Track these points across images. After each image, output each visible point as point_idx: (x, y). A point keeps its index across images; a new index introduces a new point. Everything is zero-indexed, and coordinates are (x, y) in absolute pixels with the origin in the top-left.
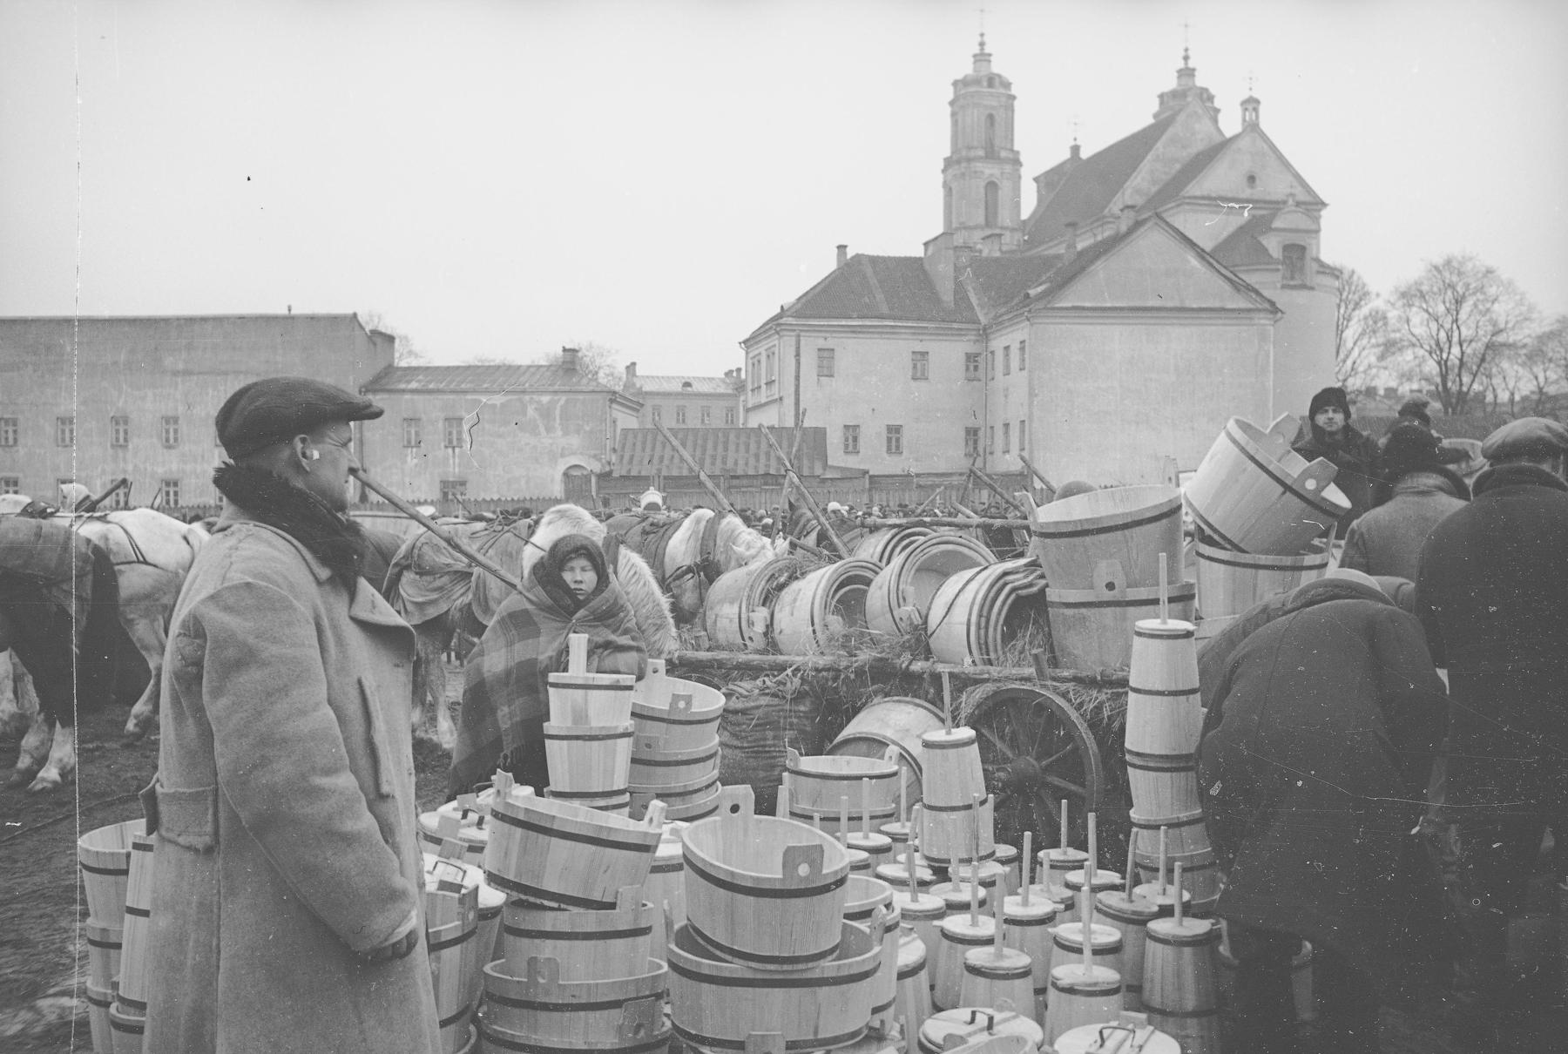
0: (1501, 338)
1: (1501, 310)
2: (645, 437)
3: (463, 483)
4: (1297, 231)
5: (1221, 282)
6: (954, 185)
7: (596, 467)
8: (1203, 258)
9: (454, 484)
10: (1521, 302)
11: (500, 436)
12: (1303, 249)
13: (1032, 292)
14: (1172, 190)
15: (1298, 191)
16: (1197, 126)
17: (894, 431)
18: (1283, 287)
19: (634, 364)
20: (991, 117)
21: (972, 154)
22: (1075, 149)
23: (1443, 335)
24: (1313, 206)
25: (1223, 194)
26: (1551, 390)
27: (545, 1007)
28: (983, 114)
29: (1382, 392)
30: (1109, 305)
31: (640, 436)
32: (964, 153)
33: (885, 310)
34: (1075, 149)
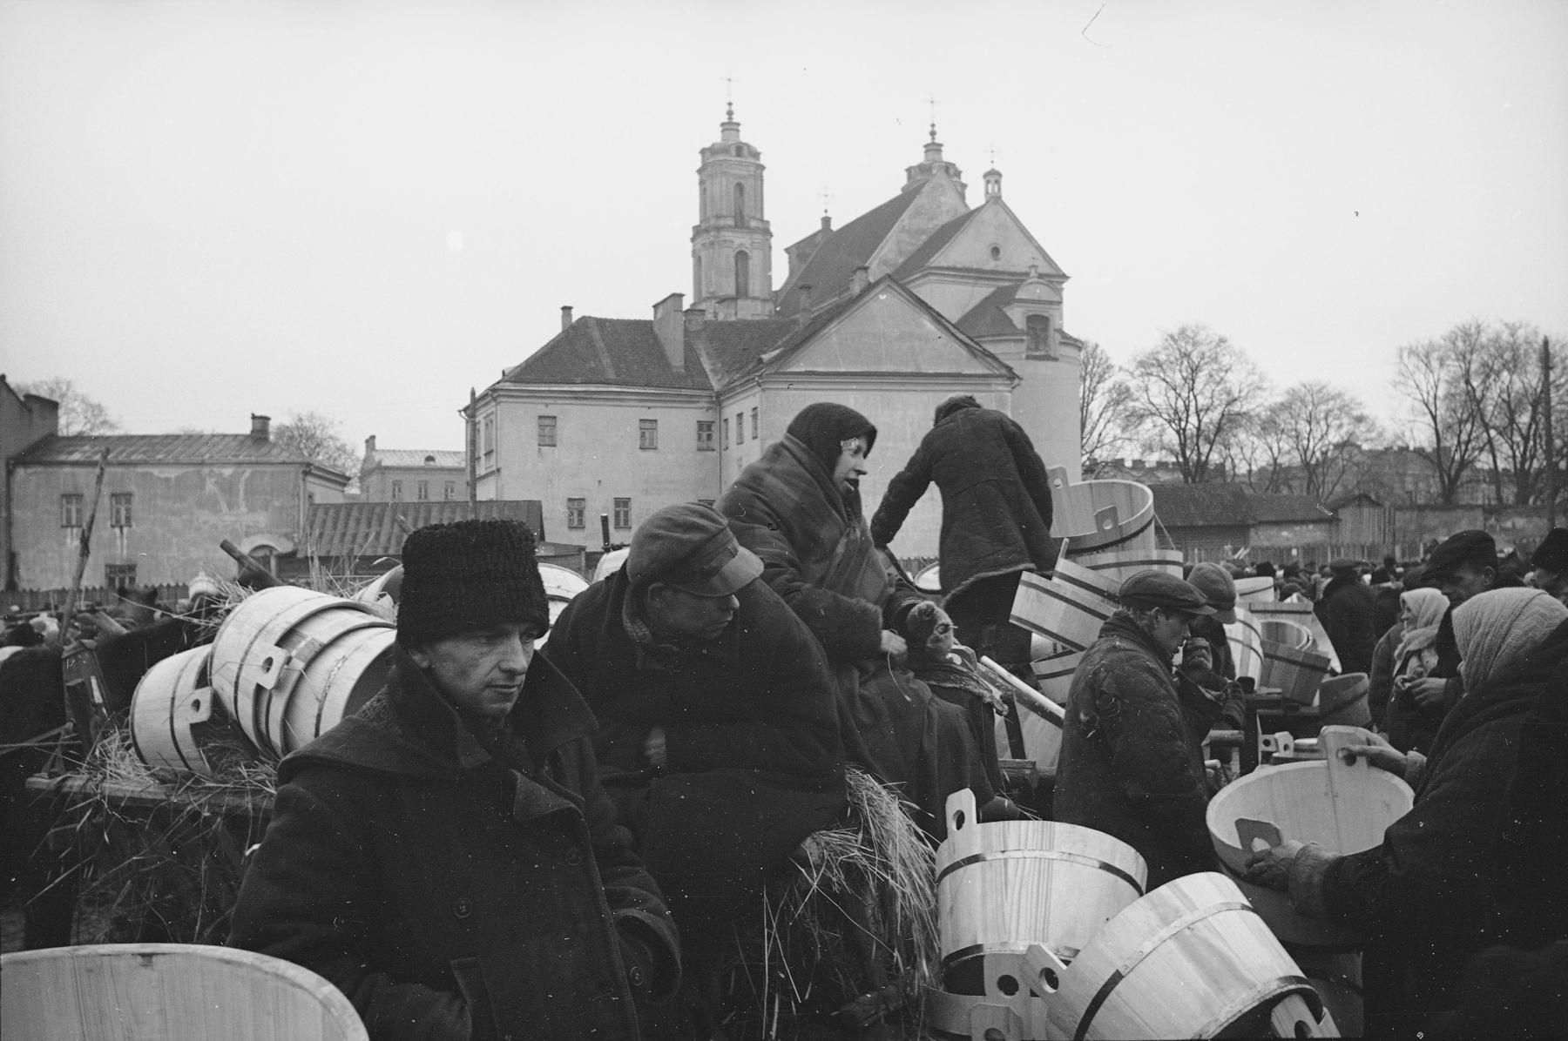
0: (1236, 408)
1: (1234, 380)
2: (337, 514)
3: (132, 568)
5: (956, 346)
6: (703, 254)
7: (284, 547)
8: (939, 323)
9: (122, 569)
10: (1252, 372)
11: (174, 513)
13: (766, 357)
14: (918, 262)
15: (1041, 263)
16: (943, 199)
17: (622, 503)
18: (1028, 358)
19: (373, 437)
20: (740, 187)
21: (722, 222)
22: (826, 221)
23: (1180, 404)
24: (1055, 278)
25: (968, 265)
26: (1284, 460)
27: (1136, 534)
28: (731, 180)
29: (1128, 464)
30: (843, 370)
31: (331, 513)
32: (713, 222)
33: (611, 375)
34: (826, 221)
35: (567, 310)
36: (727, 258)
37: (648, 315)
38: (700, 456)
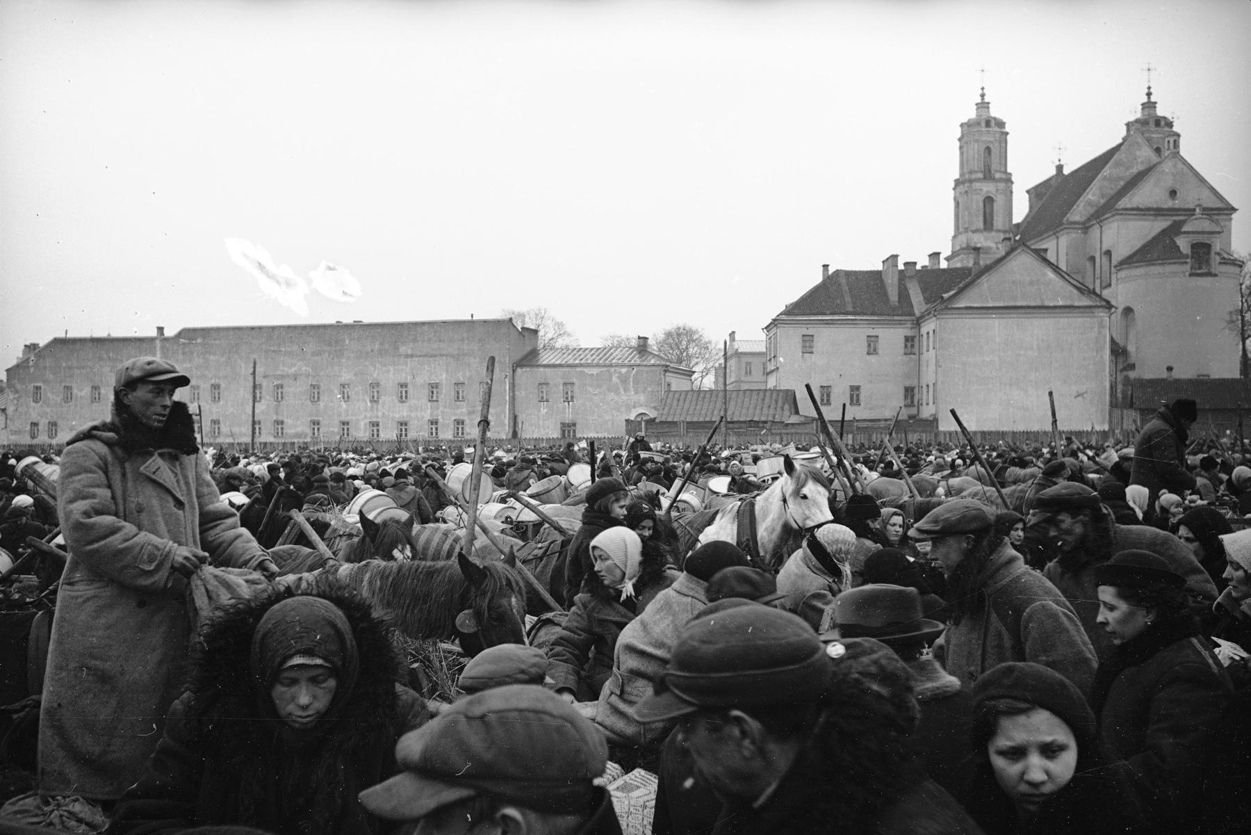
4: (1203, 233)
12: (1209, 246)
16: (1138, 153)
17: (855, 389)
18: (1191, 275)
20: (988, 150)
21: (974, 176)
22: (1060, 168)
25: (1149, 205)
34: (1060, 168)
35: (826, 267)
36: (978, 201)
37: (879, 267)
38: (906, 358)
